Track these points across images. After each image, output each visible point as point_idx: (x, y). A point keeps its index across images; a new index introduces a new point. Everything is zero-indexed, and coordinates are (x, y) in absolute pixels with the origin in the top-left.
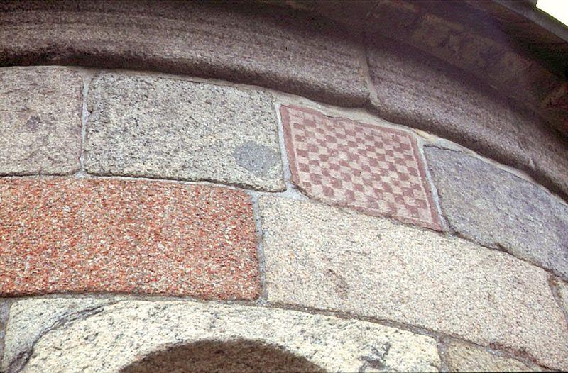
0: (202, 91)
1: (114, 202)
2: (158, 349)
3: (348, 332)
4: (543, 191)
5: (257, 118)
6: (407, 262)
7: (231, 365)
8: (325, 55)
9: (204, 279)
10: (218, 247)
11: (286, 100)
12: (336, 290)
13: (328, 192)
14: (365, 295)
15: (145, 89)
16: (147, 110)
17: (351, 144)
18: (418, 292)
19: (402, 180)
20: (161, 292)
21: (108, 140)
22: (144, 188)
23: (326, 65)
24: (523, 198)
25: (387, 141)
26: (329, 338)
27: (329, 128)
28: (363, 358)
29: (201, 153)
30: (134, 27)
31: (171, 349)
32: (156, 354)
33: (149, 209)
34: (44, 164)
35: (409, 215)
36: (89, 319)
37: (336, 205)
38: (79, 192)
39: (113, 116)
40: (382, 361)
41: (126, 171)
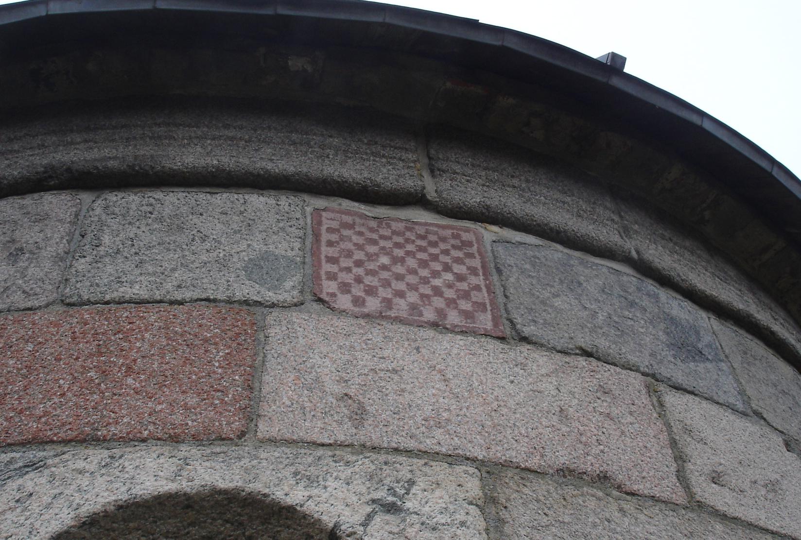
0: (219, 202)
1: (85, 334)
2: (103, 509)
3: (358, 470)
4: (650, 286)
5: (281, 225)
6: (451, 377)
7: (205, 522)
8: (374, 150)
9: (178, 418)
10: (203, 377)
12: (350, 418)
13: (358, 301)
14: (388, 422)
15: (151, 205)
16: (148, 228)
17: (398, 245)
18: (462, 413)
19: (458, 281)
20: (121, 437)
21: (94, 264)
22: (125, 315)
23: (374, 160)
24: (622, 293)
25: (444, 239)
26: (330, 479)
27: (372, 230)
28: (374, 501)
29: (203, 270)
30: (148, 139)
31: (120, 507)
32: (101, 514)
33: (126, 339)
35: (461, 322)
36: (27, 477)
37: (366, 316)
38: (48, 327)
39: (106, 239)
40: (399, 503)
41: (108, 297)
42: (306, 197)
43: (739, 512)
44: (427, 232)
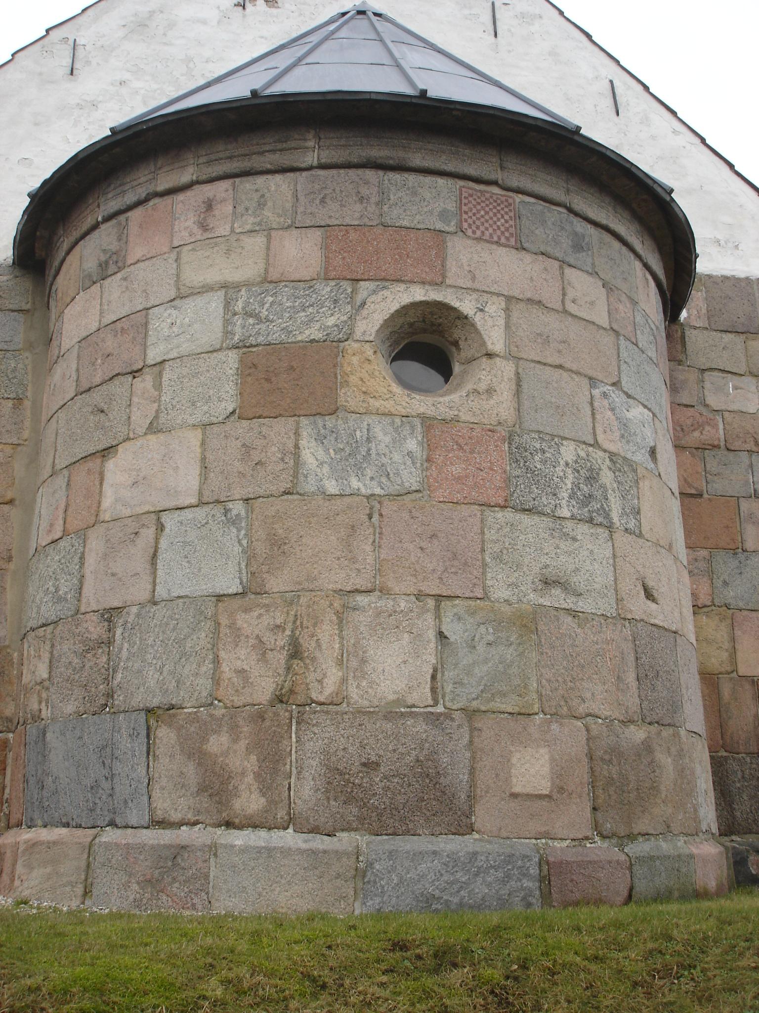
9: (424, 276)
11: (461, 183)
13: (474, 232)
27: (479, 198)
33: (405, 243)
34: (366, 220)
37: (476, 239)
39: (392, 197)
42: (457, 180)
43: (578, 314)
44: (497, 198)
